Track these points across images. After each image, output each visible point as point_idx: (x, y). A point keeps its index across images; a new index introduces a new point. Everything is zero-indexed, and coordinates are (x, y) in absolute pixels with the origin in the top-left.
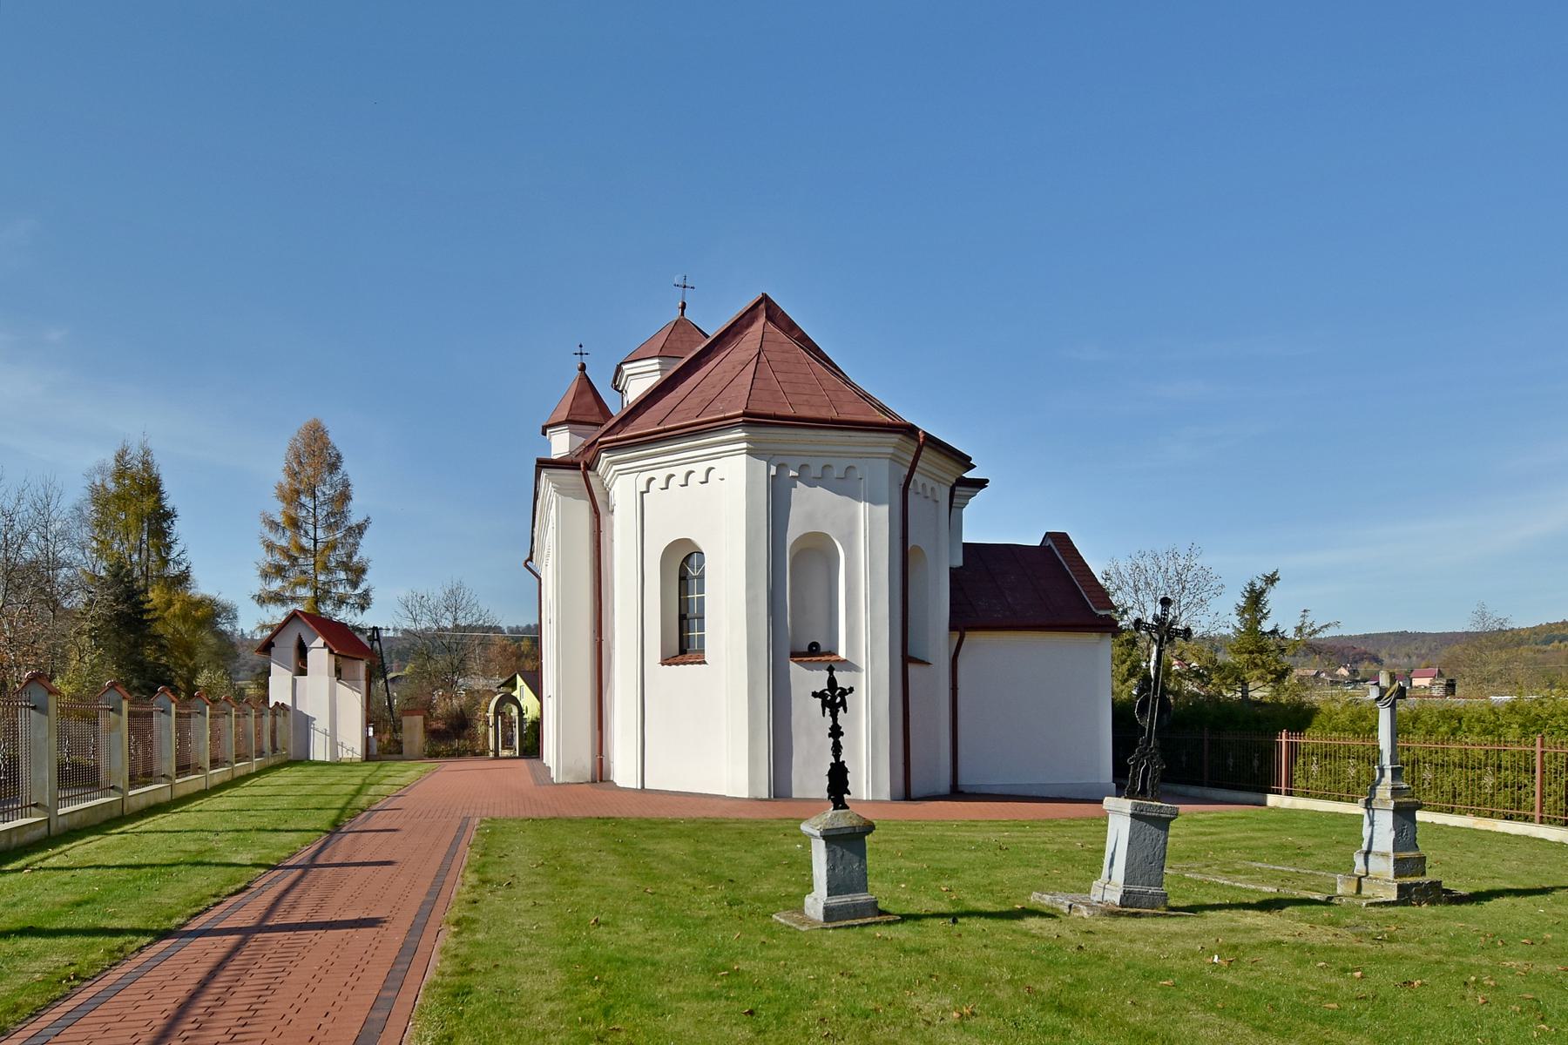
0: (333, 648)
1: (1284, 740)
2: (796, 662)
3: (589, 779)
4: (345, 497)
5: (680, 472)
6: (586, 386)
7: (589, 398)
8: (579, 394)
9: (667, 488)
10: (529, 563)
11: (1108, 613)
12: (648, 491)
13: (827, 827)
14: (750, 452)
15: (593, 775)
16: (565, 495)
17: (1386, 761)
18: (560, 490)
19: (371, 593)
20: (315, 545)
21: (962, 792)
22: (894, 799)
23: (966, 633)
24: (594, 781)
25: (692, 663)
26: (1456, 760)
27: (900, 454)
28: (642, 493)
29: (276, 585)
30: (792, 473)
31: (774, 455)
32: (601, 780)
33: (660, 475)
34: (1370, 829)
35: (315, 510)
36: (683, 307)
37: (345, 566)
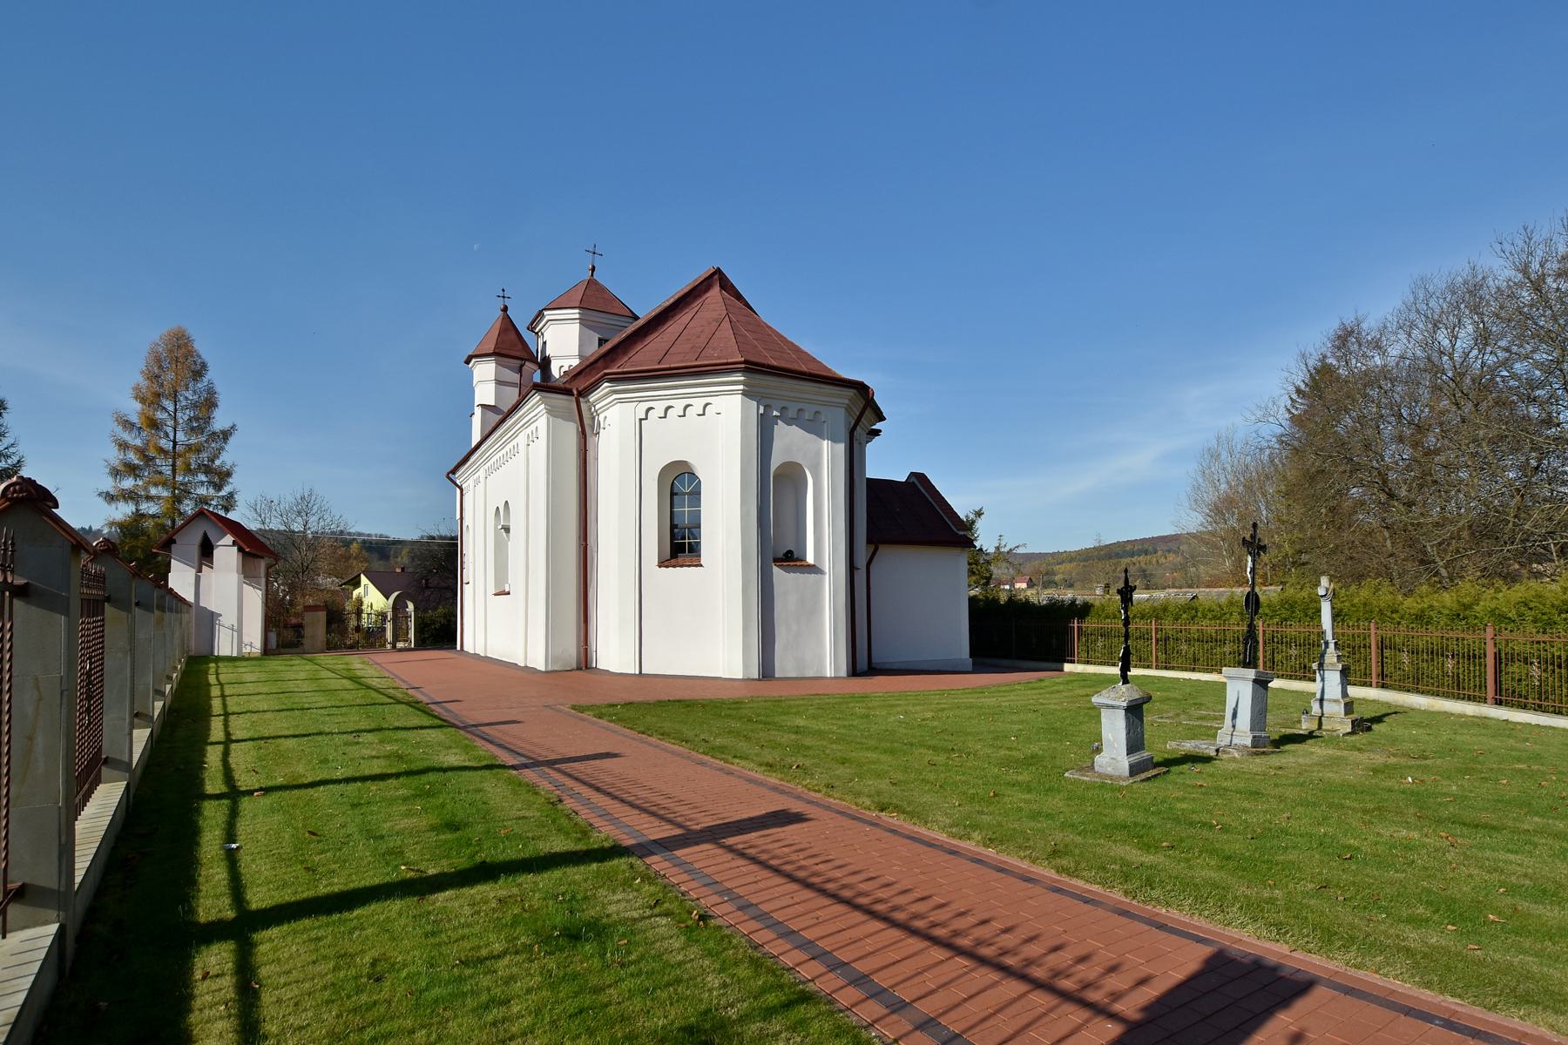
0: (245, 547)
1: (1076, 625)
2: (778, 566)
3: (574, 666)
4: (210, 403)
5: (679, 405)
6: (508, 325)
7: (513, 336)
8: (502, 332)
9: (665, 417)
10: (450, 475)
11: (965, 533)
12: (646, 419)
13: (1131, 699)
14: (745, 393)
15: (578, 663)
16: (554, 416)
17: (1329, 637)
18: (551, 412)
19: (235, 496)
20: (174, 447)
21: (875, 668)
22: (848, 676)
23: (880, 546)
24: (579, 668)
25: (689, 566)
26: (1196, 637)
27: (852, 406)
28: (641, 420)
29: (128, 483)
30: (775, 413)
31: (763, 397)
32: (586, 667)
33: (660, 407)
34: (1321, 684)
35: (175, 414)
36: (593, 269)
37: (208, 470)
